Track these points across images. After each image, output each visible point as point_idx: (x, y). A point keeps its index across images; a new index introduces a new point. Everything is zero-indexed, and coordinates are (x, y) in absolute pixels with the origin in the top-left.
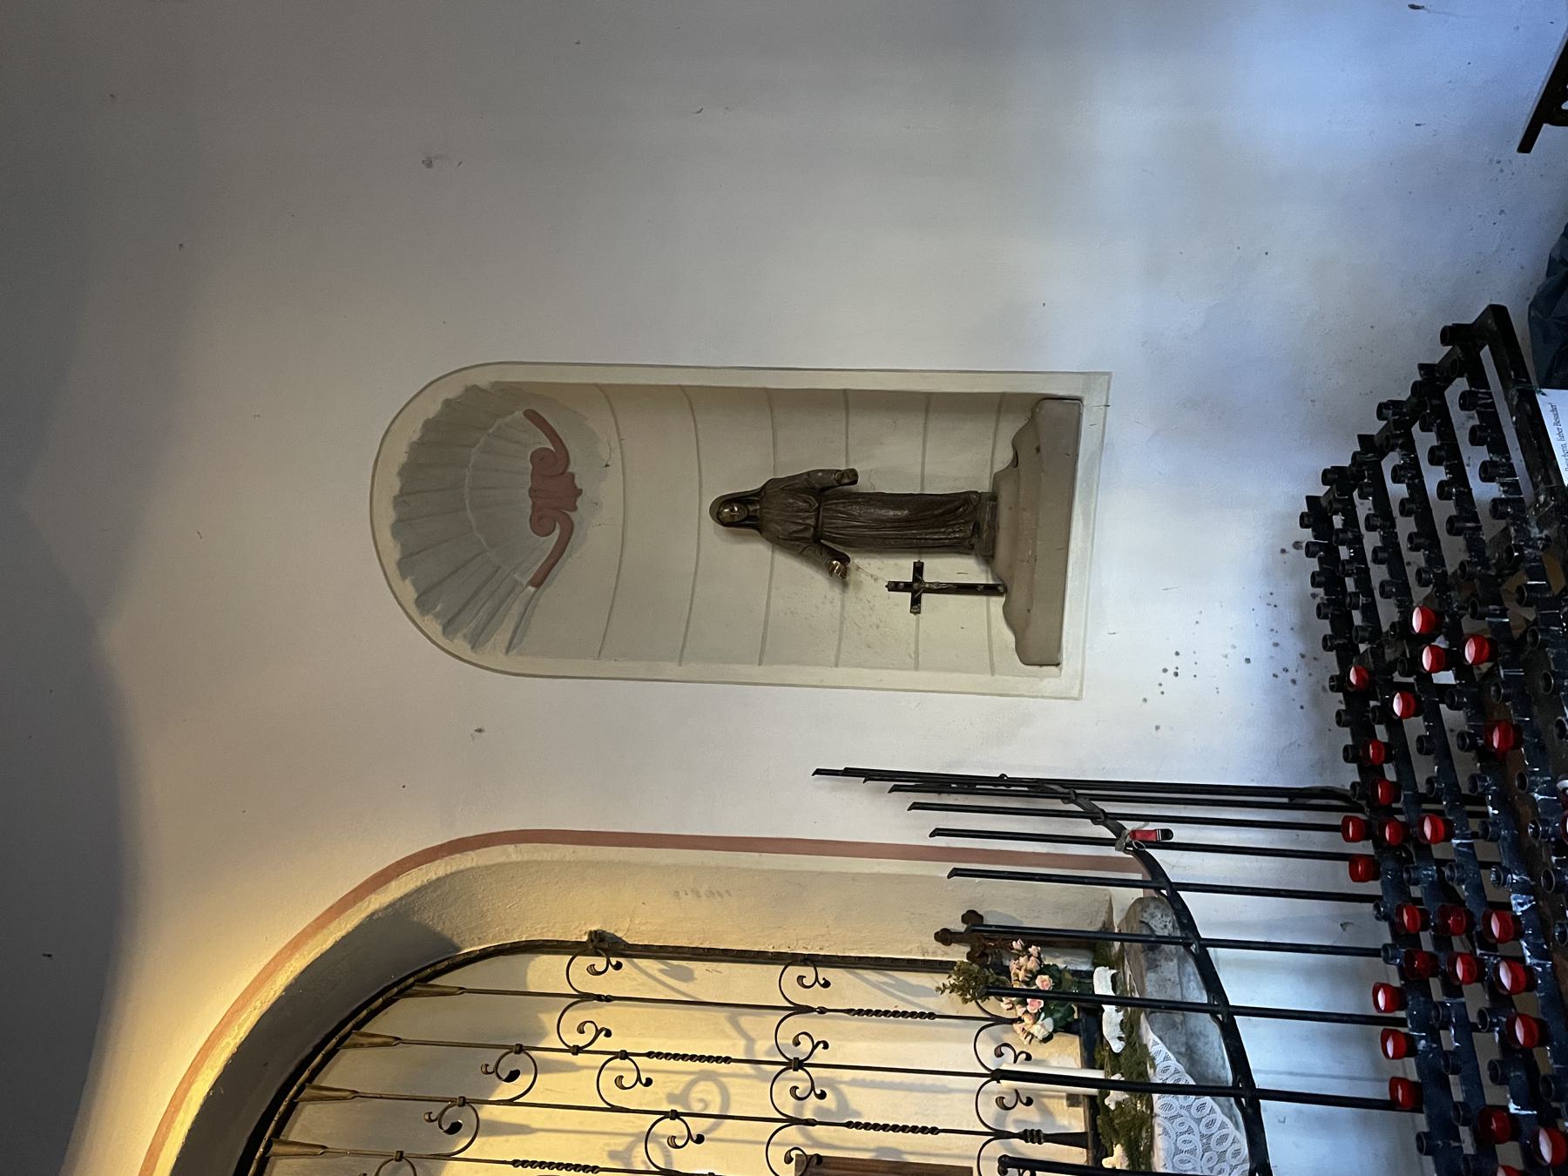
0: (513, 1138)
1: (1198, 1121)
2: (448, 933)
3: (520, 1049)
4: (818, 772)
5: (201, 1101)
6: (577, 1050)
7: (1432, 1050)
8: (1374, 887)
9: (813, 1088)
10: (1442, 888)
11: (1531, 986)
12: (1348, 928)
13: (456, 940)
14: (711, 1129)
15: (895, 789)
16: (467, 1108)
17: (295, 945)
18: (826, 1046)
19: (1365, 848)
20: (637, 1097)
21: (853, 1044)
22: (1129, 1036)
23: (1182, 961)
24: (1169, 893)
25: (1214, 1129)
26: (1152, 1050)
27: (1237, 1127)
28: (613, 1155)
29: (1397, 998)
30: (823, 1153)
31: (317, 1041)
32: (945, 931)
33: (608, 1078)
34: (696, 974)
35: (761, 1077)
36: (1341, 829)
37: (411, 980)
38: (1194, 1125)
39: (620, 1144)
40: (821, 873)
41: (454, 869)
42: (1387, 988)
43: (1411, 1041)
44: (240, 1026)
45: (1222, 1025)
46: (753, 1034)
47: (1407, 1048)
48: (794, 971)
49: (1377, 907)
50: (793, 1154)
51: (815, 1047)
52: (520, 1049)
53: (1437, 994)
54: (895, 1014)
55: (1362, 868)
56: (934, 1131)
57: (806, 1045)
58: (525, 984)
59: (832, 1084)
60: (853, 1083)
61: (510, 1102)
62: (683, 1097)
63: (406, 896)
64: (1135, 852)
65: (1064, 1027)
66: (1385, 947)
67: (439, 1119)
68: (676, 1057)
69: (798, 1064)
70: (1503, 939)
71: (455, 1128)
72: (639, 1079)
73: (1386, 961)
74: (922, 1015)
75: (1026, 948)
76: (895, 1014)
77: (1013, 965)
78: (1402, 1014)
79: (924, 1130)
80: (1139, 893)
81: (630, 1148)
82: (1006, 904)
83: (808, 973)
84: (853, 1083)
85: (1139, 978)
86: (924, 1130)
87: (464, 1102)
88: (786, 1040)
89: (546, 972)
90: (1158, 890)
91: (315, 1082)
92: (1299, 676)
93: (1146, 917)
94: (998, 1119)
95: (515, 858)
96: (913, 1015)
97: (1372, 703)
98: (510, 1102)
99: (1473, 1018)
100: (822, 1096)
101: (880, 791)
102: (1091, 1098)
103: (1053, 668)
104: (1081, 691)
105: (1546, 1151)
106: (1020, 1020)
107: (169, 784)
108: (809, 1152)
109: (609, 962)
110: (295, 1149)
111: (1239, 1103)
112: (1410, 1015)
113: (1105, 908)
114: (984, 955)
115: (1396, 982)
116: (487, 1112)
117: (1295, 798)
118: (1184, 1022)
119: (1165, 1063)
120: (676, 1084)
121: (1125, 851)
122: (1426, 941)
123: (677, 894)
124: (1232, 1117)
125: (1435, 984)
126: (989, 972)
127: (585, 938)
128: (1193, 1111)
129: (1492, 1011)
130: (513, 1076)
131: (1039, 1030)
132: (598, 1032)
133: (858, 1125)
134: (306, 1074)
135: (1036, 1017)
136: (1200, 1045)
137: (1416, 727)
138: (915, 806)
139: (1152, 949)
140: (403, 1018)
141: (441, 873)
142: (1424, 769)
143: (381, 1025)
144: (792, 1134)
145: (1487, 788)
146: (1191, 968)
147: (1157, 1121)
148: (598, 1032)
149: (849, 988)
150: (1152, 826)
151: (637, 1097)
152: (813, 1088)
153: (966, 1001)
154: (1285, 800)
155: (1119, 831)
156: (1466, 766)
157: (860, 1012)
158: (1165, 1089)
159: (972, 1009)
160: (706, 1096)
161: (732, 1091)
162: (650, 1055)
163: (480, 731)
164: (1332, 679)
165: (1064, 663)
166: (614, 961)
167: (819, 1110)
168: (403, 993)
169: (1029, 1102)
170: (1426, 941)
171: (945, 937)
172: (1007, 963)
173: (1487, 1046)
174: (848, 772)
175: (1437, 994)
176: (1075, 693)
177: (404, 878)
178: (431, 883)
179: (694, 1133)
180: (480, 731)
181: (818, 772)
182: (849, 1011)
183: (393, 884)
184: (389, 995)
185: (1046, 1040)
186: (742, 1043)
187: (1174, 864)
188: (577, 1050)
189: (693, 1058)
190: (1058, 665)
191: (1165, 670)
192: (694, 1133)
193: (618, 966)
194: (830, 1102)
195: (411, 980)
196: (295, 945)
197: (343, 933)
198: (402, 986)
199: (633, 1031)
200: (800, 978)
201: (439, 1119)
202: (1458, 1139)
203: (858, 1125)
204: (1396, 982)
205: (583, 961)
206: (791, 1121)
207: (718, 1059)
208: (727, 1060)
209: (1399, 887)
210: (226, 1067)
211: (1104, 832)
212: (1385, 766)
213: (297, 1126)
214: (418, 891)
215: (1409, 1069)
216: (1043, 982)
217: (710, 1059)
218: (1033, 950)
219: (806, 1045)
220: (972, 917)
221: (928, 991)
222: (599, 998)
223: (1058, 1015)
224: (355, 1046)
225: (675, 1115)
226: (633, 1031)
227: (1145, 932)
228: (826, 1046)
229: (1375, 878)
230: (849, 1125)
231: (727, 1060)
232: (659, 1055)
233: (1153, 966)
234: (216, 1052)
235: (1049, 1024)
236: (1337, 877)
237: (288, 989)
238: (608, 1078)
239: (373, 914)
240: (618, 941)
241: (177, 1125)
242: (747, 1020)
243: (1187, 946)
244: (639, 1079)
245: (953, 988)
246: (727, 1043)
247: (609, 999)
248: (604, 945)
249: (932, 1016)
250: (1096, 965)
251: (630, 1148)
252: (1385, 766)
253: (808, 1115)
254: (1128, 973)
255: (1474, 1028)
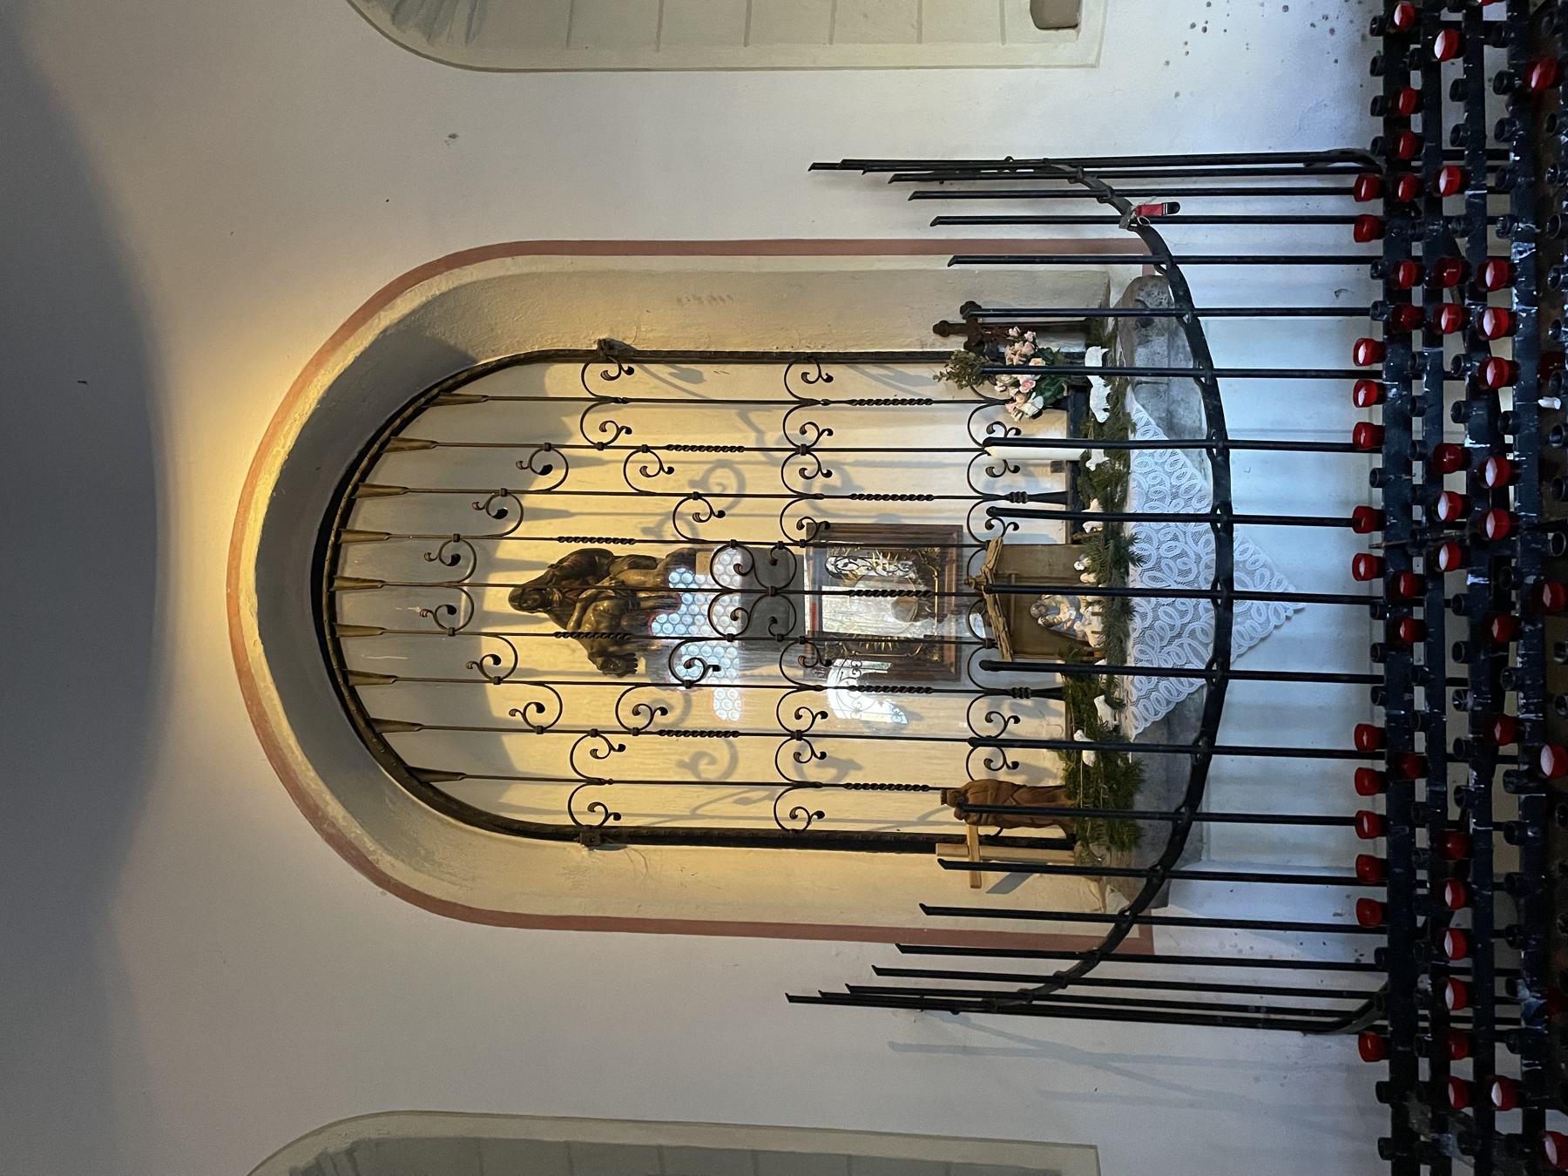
0: (555, 521)
1: (1170, 474)
2: (462, 347)
3: (549, 447)
4: (815, 167)
5: (267, 501)
6: (602, 446)
7: (1401, 396)
8: (1376, 248)
9: (820, 469)
10: (1442, 245)
11: (1511, 331)
12: (1342, 295)
13: (470, 352)
14: (731, 507)
15: (895, 179)
16: (509, 498)
17: (318, 361)
18: (831, 433)
19: (1376, 207)
20: (661, 483)
21: (853, 430)
22: (1114, 407)
23: (1173, 335)
24: (1168, 265)
25: (1184, 480)
26: (1134, 418)
27: (1205, 476)
28: (645, 531)
29: (1377, 352)
30: (830, 521)
31: (360, 447)
32: (944, 323)
33: (633, 470)
34: (705, 376)
35: (773, 463)
36: (1354, 192)
37: (436, 391)
38: (1166, 478)
39: (651, 522)
40: (822, 273)
41: (456, 284)
42: (1368, 342)
43: (1383, 389)
44: (286, 437)
45: (1204, 388)
46: (761, 427)
47: (1377, 396)
48: (798, 369)
49: (1375, 267)
50: (805, 522)
51: (820, 435)
52: (549, 447)
53: (1417, 344)
54: (895, 402)
55: (1364, 228)
56: (929, 498)
57: (812, 434)
58: (544, 390)
59: (838, 465)
60: (856, 464)
61: (548, 491)
62: (704, 481)
63: (413, 312)
64: (1139, 230)
65: (1055, 404)
66: (1375, 305)
67: (487, 506)
68: (693, 448)
69: (806, 450)
70: (1494, 287)
71: (502, 514)
72: (661, 468)
73: (1373, 319)
74: (920, 402)
75: (1021, 335)
76: (895, 402)
77: (1007, 351)
78: (1378, 367)
79: (920, 498)
80: (1137, 270)
81: (661, 524)
82: (1003, 289)
83: (812, 371)
84: (856, 464)
85: (1131, 354)
86: (920, 498)
87: (506, 493)
88: (793, 432)
89: (562, 380)
90: (1157, 265)
91: (367, 481)
92: (1341, 26)
93: (1142, 296)
94: (987, 486)
95: (514, 270)
96: (911, 402)
97: (1412, 47)
98: (548, 491)
99: (1448, 367)
100: (829, 474)
101: (877, 185)
102: (1074, 463)
103: (1071, 32)
104: (1098, 60)
105: (1490, 528)
106: (1013, 400)
107: (149, 199)
108: (818, 521)
109: (621, 368)
110: (363, 537)
111: (1210, 453)
112: (1388, 368)
113: (1102, 292)
114: (981, 343)
115: (1379, 337)
116: (529, 501)
117: (1313, 163)
118: (1168, 391)
119: (1143, 418)
120: (697, 472)
121: (1130, 228)
122: (1417, 296)
123: (679, 300)
124: (1202, 470)
125: (1417, 336)
126: (986, 360)
127: (595, 347)
128: (1167, 467)
129: (1467, 357)
130: (547, 470)
131: (1029, 409)
132: (619, 430)
133: (861, 497)
134: (357, 476)
135: (1028, 395)
136: (1181, 411)
137: (1453, 71)
138: (917, 196)
139: (1144, 326)
140: (429, 425)
141: (444, 288)
142: (1453, 115)
143: (415, 431)
144: (803, 507)
145: (1514, 133)
146: (1183, 340)
147: (1132, 476)
148: (619, 430)
149: (850, 383)
150: (1158, 201)
151: (661, 483)
152: (820, 469)
153: (961, 387)
154: (1301, 165)
155: (1124, 208)
156: (1496, 107)
157: (861, 402)
158: (1145, 815)
159: (968, 394)
160: (722, 480)
161: (747, 476)
162: (669, 447)
163: (453, 136)
164: (1374, 20)
165: (1083, 25)
166: (626, 367)
167: (826, 486)
168: (431, 402)
169: (1016, 469)
170: (1417, 296)
171: (943, 329)
172: (1002, 350)
173: (1455, 392)
174: (847, 165)
175: (1417, 344)
176: (1091, 60)
177: (408, 294)
178: (436, 299)
179: (716, 511)
180: (453, 136)
181: (815, 167)
182: (851, 402)
183: (399, 301)
184: (418, 404)
185: (1035, 416)
186: (753, 435)
187: (1175, 238)
188: (602, 446)
189: (709, 448)
190: (1075, 26)
191: (1193, 26)
192: (716, 511)
193: (630, 371)
194: (835, 479)
195: (436, 391)
196: (318, 361)
197: (361, 349)
198: (428, 396)
199: (650, 427)
200: (804, 375)
201: (487, 506)
202: (1409, 472)
203: (861, 497)
204: (1379, 337)
205: (596, 369)
206: (802, 496)
207: (732, 449)
208: (741, 449)
209: (1397, 248)
210: (282, 472)
211: (1110, 210)
212: (1413, 73)
213: (360, 517)
214: (426, 306)
215: (1376, 415)
216: (1037, 362)
217: (724, 449)
218: (1029, 335)
219: (812, 434)
220: (970, 309)
221: (926, 380)
222: (616, 400)
223: (1048, 394)
224: (396, 450)
225: (697, 496)
226: (650, 427)
227: (1140, 306)
228: (831, 433)
229: (1378, 237)
230: (853, 497)
231: (741, 449)
232: (677, 448)
233: (1145, 341)
234: (269, 459)
235: (1039, 402)
236: (1340, 239)
237: (322, 401)
238: (633, 470)
239: (385, 330)
240: (628, 348)
241: (251, 521)
242: (757, 416)
243: (1180, 317)
244: (661, 468)
245: (950, 376)
246: (739, 436)
247: (625, 401)
248: (612, 352)
249: (929, 402)
250: (1088, 346)
251: (661, 524)
252: (1413, 73)
253: (816, 491)
254: (1119, 349)
255: (1448, 376)
